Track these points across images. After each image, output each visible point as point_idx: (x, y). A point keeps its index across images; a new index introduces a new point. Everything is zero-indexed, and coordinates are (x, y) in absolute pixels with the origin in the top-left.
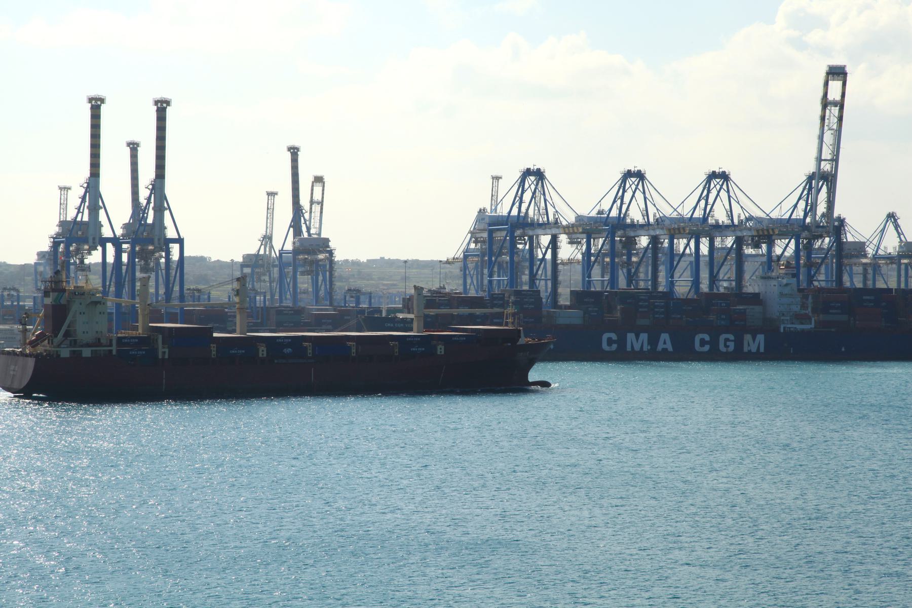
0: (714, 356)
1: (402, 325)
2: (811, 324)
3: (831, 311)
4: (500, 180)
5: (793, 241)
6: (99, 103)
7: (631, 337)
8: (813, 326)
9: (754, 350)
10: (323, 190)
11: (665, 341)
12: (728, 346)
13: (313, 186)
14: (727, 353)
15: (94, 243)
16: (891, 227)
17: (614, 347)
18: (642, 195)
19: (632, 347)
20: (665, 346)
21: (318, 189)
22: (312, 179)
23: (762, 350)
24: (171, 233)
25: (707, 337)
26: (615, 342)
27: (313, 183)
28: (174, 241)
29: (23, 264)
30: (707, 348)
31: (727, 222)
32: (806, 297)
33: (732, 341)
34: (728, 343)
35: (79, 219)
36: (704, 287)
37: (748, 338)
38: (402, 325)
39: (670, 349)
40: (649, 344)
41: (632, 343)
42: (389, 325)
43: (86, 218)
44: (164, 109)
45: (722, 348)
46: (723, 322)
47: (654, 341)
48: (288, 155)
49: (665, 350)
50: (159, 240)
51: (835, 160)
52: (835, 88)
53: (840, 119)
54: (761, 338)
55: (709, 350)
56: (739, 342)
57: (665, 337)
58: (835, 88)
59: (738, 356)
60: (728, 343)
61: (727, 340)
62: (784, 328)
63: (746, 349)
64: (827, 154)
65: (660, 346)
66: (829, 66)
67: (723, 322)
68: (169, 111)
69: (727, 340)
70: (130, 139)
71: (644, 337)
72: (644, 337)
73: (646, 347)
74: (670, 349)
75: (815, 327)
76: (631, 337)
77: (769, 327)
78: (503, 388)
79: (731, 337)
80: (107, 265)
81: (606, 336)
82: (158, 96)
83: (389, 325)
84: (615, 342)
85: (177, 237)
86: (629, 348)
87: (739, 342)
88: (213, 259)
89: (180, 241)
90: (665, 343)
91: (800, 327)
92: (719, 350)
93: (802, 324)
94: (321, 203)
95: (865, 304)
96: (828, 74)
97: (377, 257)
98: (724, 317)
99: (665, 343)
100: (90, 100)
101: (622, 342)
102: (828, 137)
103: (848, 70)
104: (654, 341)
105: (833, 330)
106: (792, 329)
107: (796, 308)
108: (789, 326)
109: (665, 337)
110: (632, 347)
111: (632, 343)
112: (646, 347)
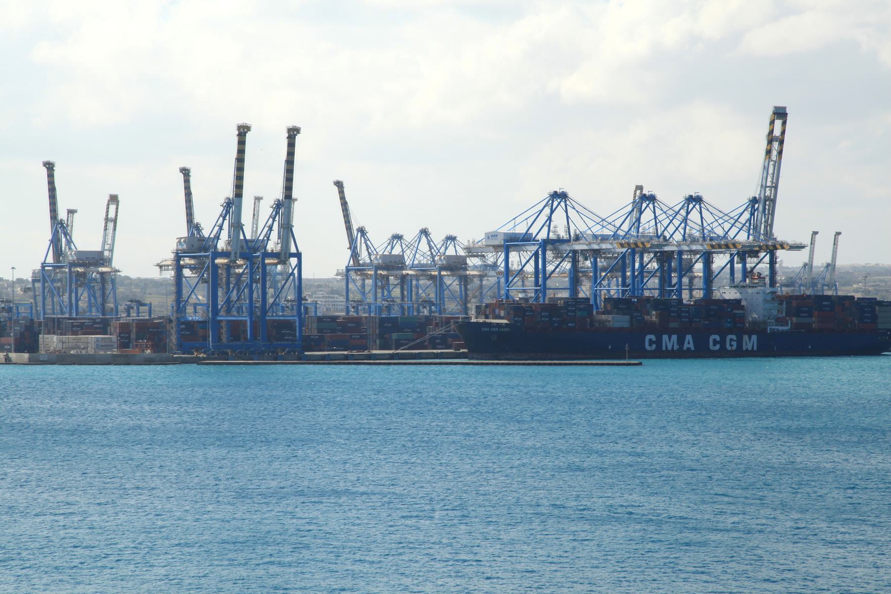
0: (723, 354)
1: (497, 329)
2: (788, 325)
3: (801, 315)
4: (261, 201)
5: (768, 256)
6: (246, 130)
7: (665, 337)
8: (789, 327)
9: (750, 349)
10: (117, 208)
11: (689, 342)
13: (108, 205)
14: (732, 351)
15: (235, 257)
16: (424, 239)
17: (654, 346)
18: (699, 215)
20: (689, 346)
21: (112, 208)
22: (107, 198)
23: (755, 349)
27: (109, 201)
28: (293, 255)
30: (718, 347)
31: (566, 237)
32: (781, 304)
33: (735, 341)
34: (733, 343)
38: (497, 329)
39: (693, 348)
40: (678, 344)
42: (486, 329)
45: (729, 348)
46: (728, 325)
47: (681, 342)
48: (181, 176)
50: (285, 254)
51: (775, 187)
53: (780, 153)
54: (754, 337)
55: (656, 348)
56: (740, 342)
57: (689, 338)
59: (740, 353)
61: (731, 340)
63: (744, 348)
65: (686, 346)
66: (775, 107)
67: (728, 325)
69: (731, 340)
70: (46, 159)
71: (674, 337)
72: (674, 337)
73: (676, 347)
74: (693, 348)
75: (791, 329)
77: (758, 329)
79: (734, 337)
81: (648, 337)
83: (486, 329)
85: (296, 252)
86: (664, 349)
87: (740, 342)
88: (122, 274)
89: (298, 255)
90: (689, 343)
91: (781, 328)
92: (645, 349)
93: (783, 326)
94: (115, 221)
95: (824, 309)
98: (729, 320)
99: (689, 343)
100: (239, 127)
101: (659, 342)
103: (788, 111)
104: (681, 342)
105: (803, 331)
106: (775, 330)
107: (775, 312)
108: (774, 327)
109: (689, 338)
112: (676, 347)
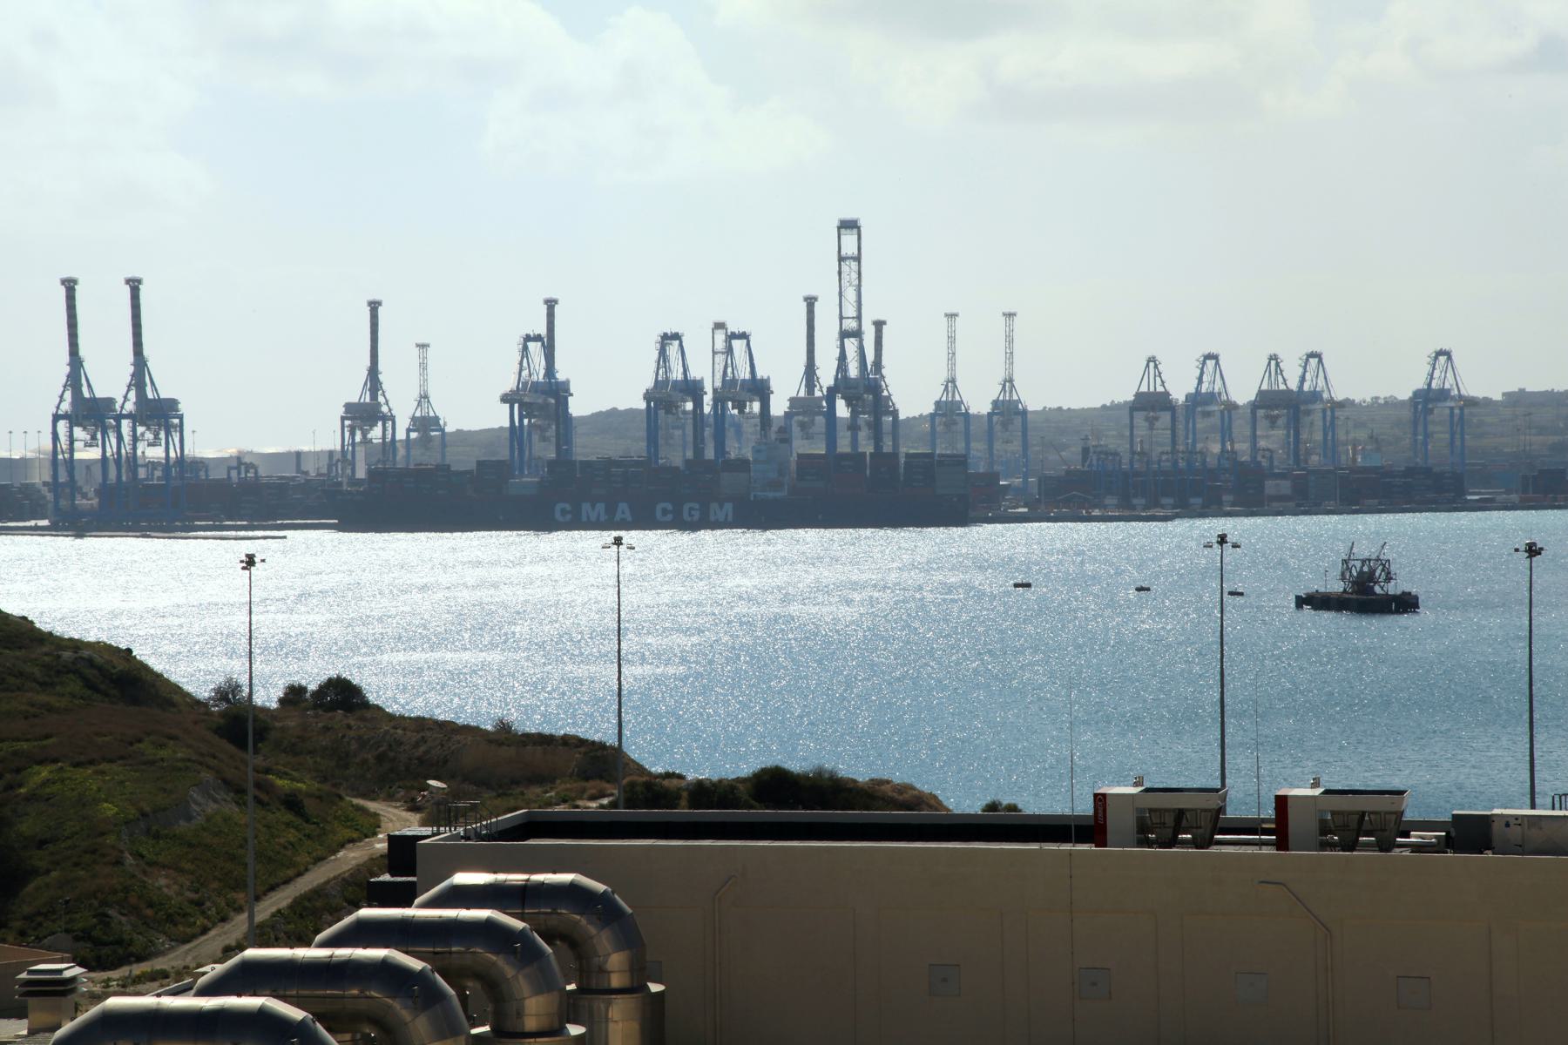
12: (693, 515)
19: (588, 517)
24: (385, 409)
25: (669, 507)
26: (569, 512)
29: (496, 426)
34: (693, 512)
35: (362, 401)
36: (710, 453)
37: (714, 506)
41: (587, 512)
43: (368, 400)
44: (377, 308)
45: (686, 517)
49: (623, 520)
52: (849, 246)
57: (623, 506)
58: (849, 246)
60: (693, 512)
61: (691, 509)
62: (755, 496)
64: (850, 311)
68: (557, 309)
69: (691, 509)
72: (601, 507)
76: (586, 507)
78: (985, 505)
79: (696, 506)
80: (838, 421)
81: (559, 507)
82: (371, 298)
84: (569, 512)
90: (623, 513)
91: (771, 495)
96: (839, 228)
97: (1055, 405)
99: (623, 513)
102: (850, 294)
108: (759, 493)
109: (623, 506)
110: (588, 517)
111: (587, 512)
112: (603, 518)
